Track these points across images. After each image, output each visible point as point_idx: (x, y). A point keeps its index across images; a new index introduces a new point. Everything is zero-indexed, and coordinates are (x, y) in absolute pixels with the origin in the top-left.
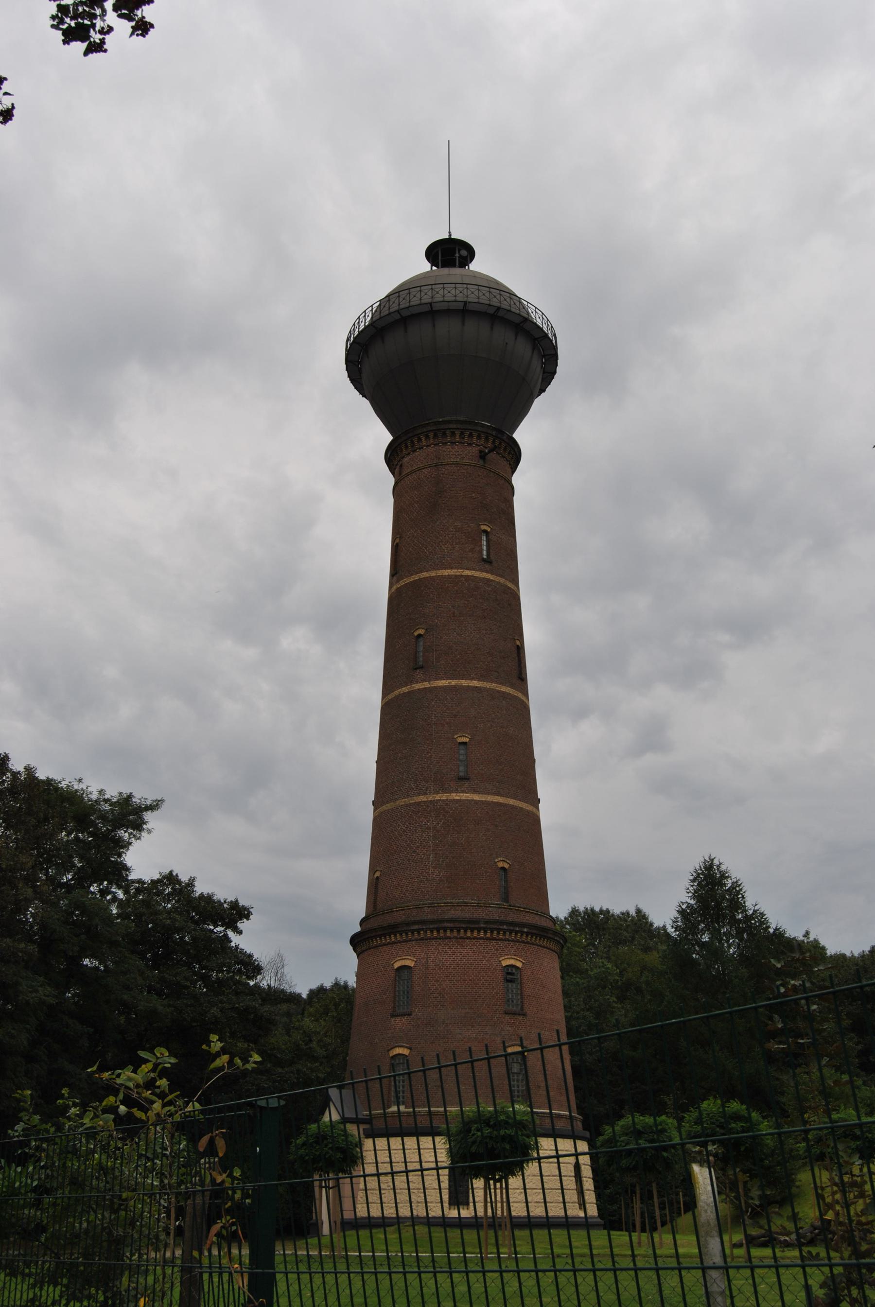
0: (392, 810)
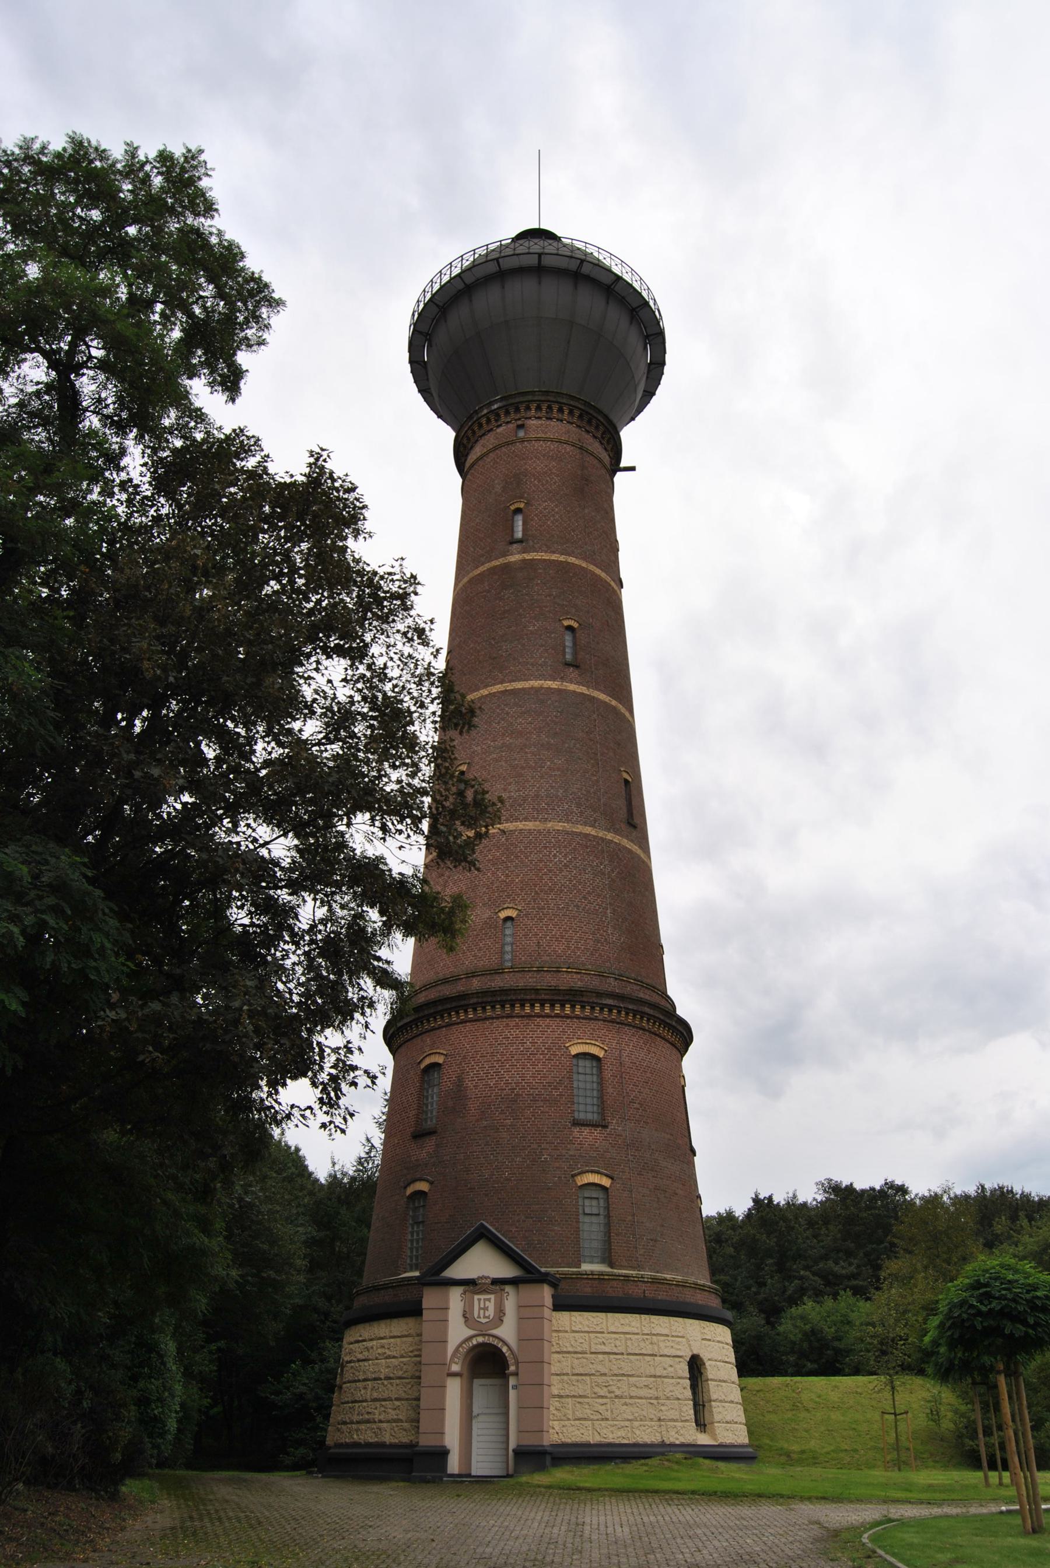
0: (539, 831)
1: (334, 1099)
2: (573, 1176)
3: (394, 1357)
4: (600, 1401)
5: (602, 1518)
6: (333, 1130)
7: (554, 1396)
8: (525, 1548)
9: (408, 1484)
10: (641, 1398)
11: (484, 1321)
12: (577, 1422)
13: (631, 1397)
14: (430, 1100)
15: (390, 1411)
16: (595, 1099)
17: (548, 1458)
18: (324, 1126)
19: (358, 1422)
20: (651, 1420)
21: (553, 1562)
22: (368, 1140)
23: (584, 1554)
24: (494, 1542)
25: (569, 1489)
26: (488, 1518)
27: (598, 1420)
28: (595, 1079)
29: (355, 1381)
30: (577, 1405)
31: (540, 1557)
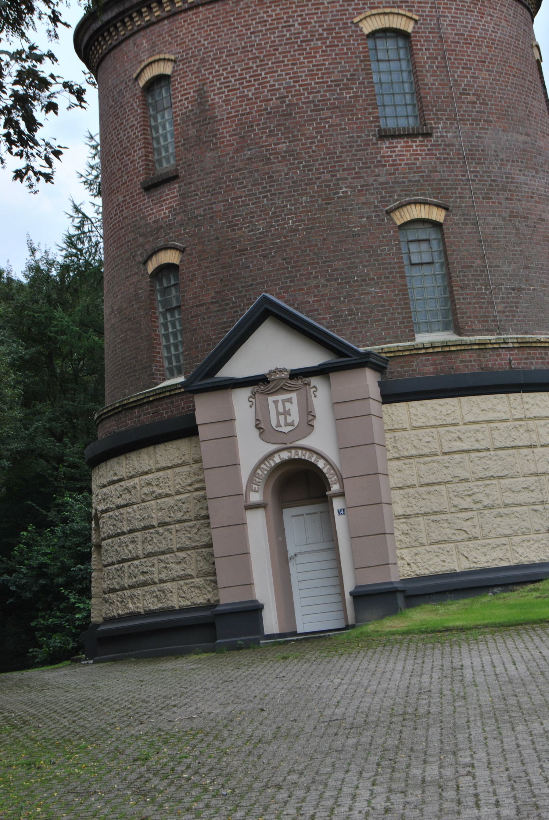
1: (26, 132)
2: (388, 213)
3: (167, 495)
4: (464, 515)
5: (486, 659)
6: (34, 179)
7: (398, 517)
8: (388, 703)
9: (212, 654)
10: (520, 505)
11: (286, 429)
12: (434, 547)
13: (506, 506)
14: (161, 132)
15: (173, 566)
16: (408, 97)
17: (400, 599)
18: (19, 175)
19: (131, 587)
20: (538, 532)
21: (429, 713)
22: (77, 210)
23: (469, 700)
24: (345, 702)
25: (434, 631)
26: (331, 677)
27: (463, 541)
28: (404, 64)
29: (118, 535)
30: (432, 524)
31: (410, 710)
